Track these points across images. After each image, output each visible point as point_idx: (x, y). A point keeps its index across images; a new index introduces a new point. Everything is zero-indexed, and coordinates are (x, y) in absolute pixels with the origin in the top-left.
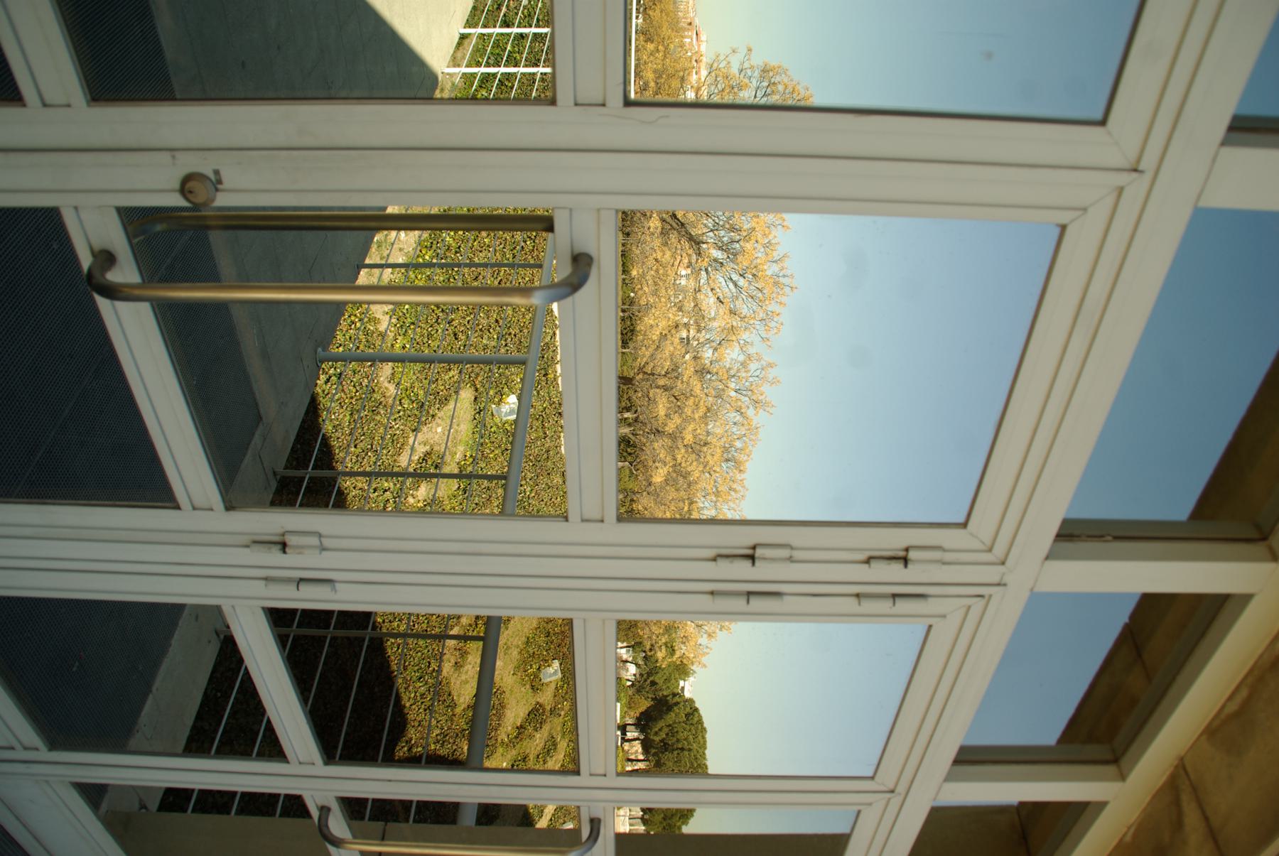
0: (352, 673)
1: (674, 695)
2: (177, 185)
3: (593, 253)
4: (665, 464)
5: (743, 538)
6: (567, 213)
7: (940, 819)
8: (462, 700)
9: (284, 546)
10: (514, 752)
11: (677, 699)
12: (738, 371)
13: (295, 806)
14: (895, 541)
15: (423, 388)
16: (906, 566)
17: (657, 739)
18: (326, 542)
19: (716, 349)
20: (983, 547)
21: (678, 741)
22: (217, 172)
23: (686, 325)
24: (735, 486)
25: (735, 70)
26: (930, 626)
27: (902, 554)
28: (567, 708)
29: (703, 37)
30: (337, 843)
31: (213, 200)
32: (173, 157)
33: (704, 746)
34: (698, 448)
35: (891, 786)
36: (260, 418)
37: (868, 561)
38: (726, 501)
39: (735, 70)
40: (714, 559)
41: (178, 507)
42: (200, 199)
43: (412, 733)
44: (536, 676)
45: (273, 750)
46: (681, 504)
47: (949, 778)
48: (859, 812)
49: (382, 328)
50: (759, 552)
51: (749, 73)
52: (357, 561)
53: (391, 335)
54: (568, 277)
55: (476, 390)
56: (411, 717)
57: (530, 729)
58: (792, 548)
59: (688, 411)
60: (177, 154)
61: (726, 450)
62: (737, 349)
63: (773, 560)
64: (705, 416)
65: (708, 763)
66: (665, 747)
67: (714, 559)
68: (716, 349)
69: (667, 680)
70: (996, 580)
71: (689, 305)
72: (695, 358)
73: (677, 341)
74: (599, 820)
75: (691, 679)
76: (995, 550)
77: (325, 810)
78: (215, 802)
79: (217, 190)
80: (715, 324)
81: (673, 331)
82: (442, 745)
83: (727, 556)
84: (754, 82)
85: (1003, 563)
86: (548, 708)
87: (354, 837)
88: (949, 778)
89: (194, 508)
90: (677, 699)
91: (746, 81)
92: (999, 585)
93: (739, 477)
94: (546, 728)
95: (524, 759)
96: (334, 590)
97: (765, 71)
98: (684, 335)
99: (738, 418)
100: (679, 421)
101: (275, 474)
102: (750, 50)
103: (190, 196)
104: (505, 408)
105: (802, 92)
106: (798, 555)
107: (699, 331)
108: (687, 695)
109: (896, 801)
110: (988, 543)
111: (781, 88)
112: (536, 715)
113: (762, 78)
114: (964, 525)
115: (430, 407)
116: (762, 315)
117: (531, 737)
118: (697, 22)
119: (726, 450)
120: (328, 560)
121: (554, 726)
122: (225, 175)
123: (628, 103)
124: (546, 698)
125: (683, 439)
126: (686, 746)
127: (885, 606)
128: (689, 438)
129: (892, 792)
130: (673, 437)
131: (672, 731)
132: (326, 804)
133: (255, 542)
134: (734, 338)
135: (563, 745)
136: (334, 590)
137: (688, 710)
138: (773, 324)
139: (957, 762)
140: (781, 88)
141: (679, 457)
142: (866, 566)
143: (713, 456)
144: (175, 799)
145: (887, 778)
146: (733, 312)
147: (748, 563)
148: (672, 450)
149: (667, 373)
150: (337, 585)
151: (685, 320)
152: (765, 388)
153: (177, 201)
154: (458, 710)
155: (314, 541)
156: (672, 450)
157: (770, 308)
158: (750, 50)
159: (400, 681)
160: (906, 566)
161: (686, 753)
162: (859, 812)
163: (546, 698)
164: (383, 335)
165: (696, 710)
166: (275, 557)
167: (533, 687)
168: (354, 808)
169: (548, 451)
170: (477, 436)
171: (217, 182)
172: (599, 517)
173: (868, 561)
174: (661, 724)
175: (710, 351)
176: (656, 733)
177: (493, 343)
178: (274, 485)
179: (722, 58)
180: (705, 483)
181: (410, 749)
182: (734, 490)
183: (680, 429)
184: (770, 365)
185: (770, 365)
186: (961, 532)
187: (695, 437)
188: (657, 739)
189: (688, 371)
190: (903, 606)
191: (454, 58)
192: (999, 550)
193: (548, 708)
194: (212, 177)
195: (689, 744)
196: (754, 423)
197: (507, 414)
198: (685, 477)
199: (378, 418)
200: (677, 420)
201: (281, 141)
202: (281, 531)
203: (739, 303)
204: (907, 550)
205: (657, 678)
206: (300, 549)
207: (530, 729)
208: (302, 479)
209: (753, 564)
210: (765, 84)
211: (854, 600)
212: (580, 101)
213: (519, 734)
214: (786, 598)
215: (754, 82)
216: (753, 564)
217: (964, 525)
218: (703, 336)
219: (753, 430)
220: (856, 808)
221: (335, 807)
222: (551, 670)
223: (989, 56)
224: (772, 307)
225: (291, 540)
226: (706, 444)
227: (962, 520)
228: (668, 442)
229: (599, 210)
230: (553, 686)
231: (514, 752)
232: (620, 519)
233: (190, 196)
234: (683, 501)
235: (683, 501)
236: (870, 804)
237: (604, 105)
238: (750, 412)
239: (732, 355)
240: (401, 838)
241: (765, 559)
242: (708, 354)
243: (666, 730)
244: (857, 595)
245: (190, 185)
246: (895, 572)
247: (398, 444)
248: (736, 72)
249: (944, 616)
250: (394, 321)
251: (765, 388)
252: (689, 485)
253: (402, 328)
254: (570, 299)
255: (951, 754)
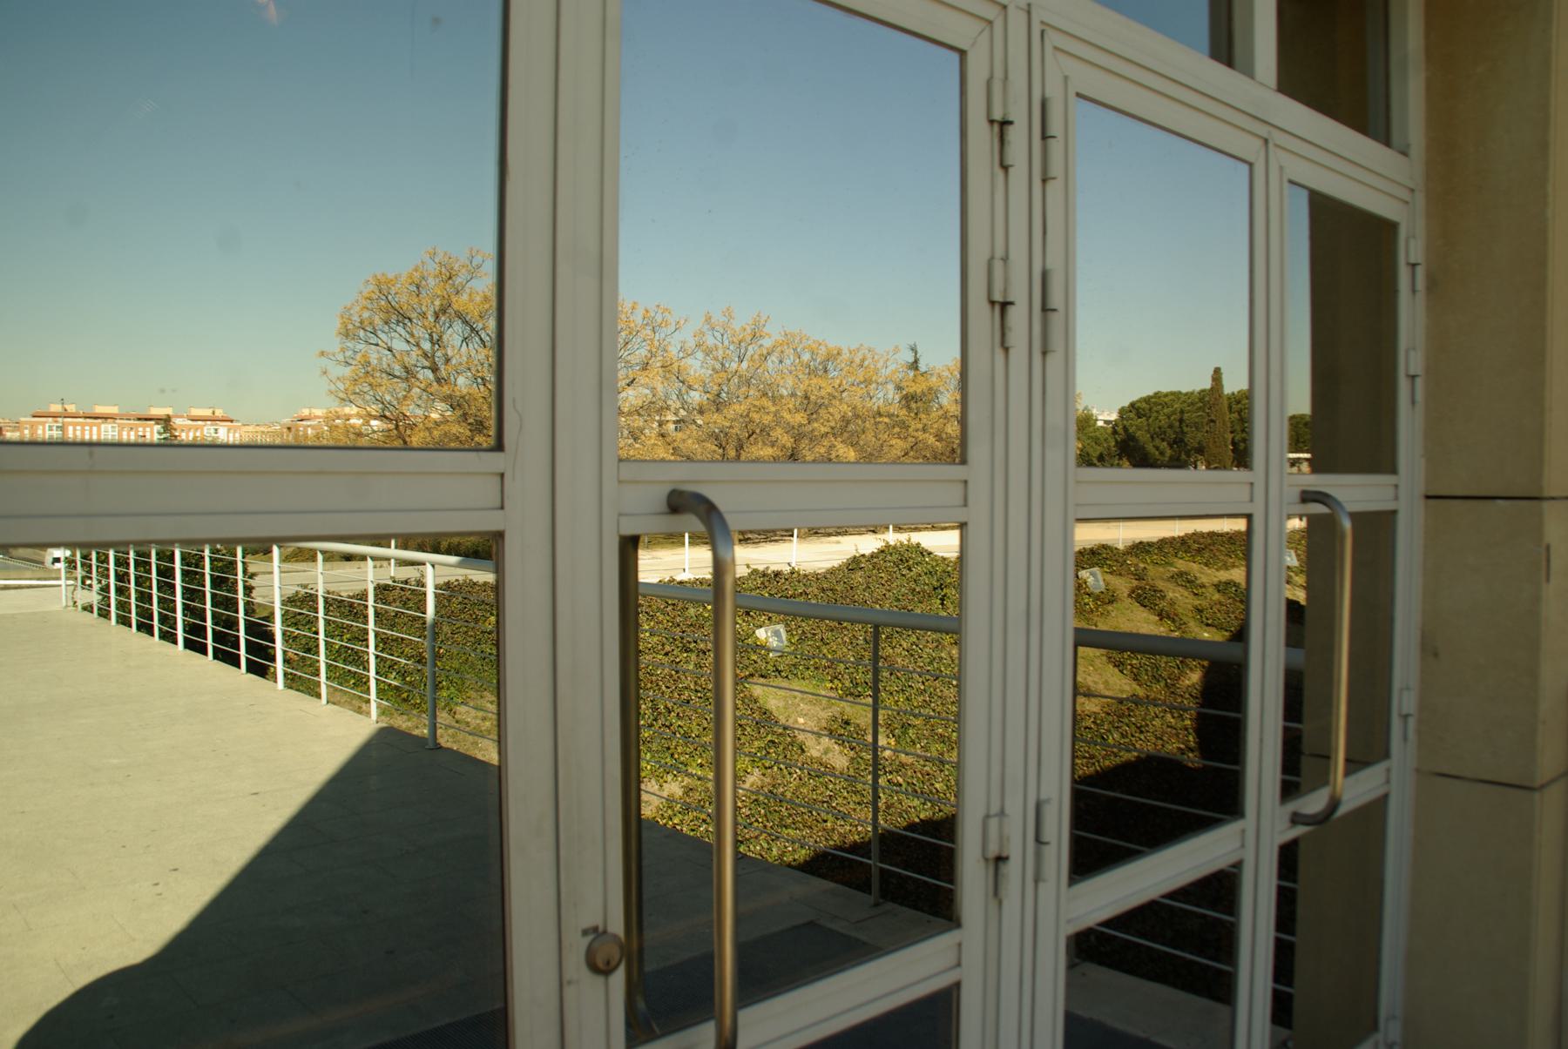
0: (1118, 809)
1: (1115, 432)
2: (600, 980)
3: (667, 489)
4: (832, 446)
5: (982, 317)
6: (623, 520)
7: (1292, 83)
8: (1127, 688)
9: (1000, 859)
10: (1192, 624)
11: (1120, 429)
12: (716, 359)
13: (1288, 856)
14: (981, 136)
15: (751, 743)
16: (1011, 123)
17: (1169, 452)
18: (995, 809)
19: (690, 387)
20: (986, 34)
21: (1171, 426)
22: (585, 933)
23: (661, 424)
24: (857, 361)
25: (347, 371)
26: (1078, 95)
27: (996, 128)
28: (1135, 560)
29: (306, 412)
30: (1334, 804)
31: (615, 936)
32: (569, 983)
33: (1176, 395)
34: (811, 406)
35: (1259, 143)
36: (811, 924)
37: (1005, 168)
38: (876, 372)
39: (347, 371)
40: (1006, 350)
41: (958, 985)
42: (615, 953)
43: (1172, 747)
44: (1097, 598)
45: (1220, 888)
46: (881, 427)
47: (1249, 73)
48: (1291, 182)
49: (679, 792)
50: (998, 297)
51: (349, 353)
52: (1011, 779)
53: (687, 780)
54: (697, 515)
55: (752, 675)
56: (1151, 748)
57: (1163, 604)
58: (992, 258)
59: (767, 419)
60: (567, 977)
61: (812, 372)
62: (689, 361)
63: (1006, 280)
64: (773, 399)
65: (1198, 389)
66: (1178, 442)
67: (1006, 350)
68: (690, 387)
69: (1097, 441)
70: (1023, 17)
71: (638, 422)
72: (701, 412)
73: (680, 435)
74: (1304, 492)
75: (1094, 411)
76: (991, 17)
77: (1296, 819)
78: (1284, 957)
79: (605, 932)
80: (660, 388)
81: (669, 439)
82: (1185, 710)
83: (1003, 335)
84: (359, 347)
85: (1005, 7)
86: (1135, 583)
87: (1325, 783)
88: (1249, 73)
89: (959, 965)
90: (1120, 429)
91: (358, 357)
92: (1029, 13)
93: (846, 355)
94: (1160, 584)
95: (1200, 611)
96: (1048, 801)
97: (346, 334)
98: (672, 426)
99: (774, 358)
100: (779, 431)
101: (876, 905)
102: (322, 353)
103: (613, 963)
104: (773, 642)
105: (371, 287)
106: (999, 253)
107: (668, 408)
108: (1114, 417)
109: (1278, 138)
110: (983, 25)
111: (366, 315)
112: (1146, 597)
113: (356, 337)
114: (962, 53)
115: (774, 733)
116: (648, 331)
117: (1172, 603)
118: (287, 421)
119: (812, 372)
120: (1014, 807)
121: (1157, 575)
122: (588, 923)
123: (499, 446)
124: (1123, 585)
125: (800, 425)
126: (1178, 416)
127: (1056, 147)
128: (800, 418)
129: (1266, 141)
130: (798, 438)
131: (1159, 434)
132: (1287, 818)
133: (996, 892)
134: (675, 366)
135: (1181, 564)
136: (1048, 801)
137: (1132, 415)
138: (659, 319)
139: (1229, 62)
140: (366, 315)
141: (823, 430)
142: (1011, 170)
143: (822, 387)
144: (1282, 1010)
145: (1249, 147)
146: (645, 367)
147: (1011, 310)
148: (814, 439)
149: (721, 446)
150: (1043, 796)
151: (655, 425)
152: (736, 326)
153: (619, 978)
154: (1141, 692)
155: (993, 824)
156: (814, 439)
157: (639, 320)
158: (322, 353)
159: (1107, 763)
160: (1011, 123)
161: (1186, 416)
162: (1291, 182)
163: (1123, 585)
164: (689, 790)
165: (1132, 405)
166: (1012, 870)
167: (1111, 602)
168: (1289, 790)
169: (823, 590)
170: (807, 674)
171: (596, 933)
172: (961, 486)
173: (1005, 168)
174: (1150, 448)
175: (692, 393)
176: (1162, 453)
177: (693, 656)
178: (890, 906)
179: (333, 387)
180: (854, 397)
181: (1191, 750)
182: (863, 360)
183: (789, 429)
184: (708, 319)
185: (708, 319)
186: (971, 58)
187: (798, 411)
188: (1169, 452)
189: (718, 420)
190: (1055, 127)
191: (359, 711)
192: (991, 12)
193: (1135, 583)
194: (590, 937)
195: (1174, 413)
196: (780, 338)
197: (780, 640)
198: (848, 422)
199: (789, 795)
200: (778, 433)
201: (549, 856)
202: (982, 863)
203: (634, 359)
204: (992, 122)
205: (1095, 454)
206: (1002, 839)
207: (1163, 604)
208: (882, 870)
209: (1011, 303)
210: (362, 333)
211: (1050, 185)
212: (498, 504)
213: (1168, 617)
214: (1049, 266)
215: (359, 347)
216: (1011, 303)
217: (962, 53)
218: (674, 403)
219: (789, 340)
220: (1286, 184)
221: (1292, 806)
222: (1091, 580)
223: (436, 21)
224: (638, 318)
225: (993, 850)
226: (807, 397)
227: (955, 57)
228: (804, 443)
229: (620, 482)
230: (1108, 577)
231: (1192, 624)
232: (964, 462)
233: (613, 963)
234: (877, 423)
235: (877, 423)
236: (1281, 168)
237: (502, 475)
238: (767, 343)
239: (696, 367)
240: (1327, 731)
241: (1005, 290)
242: (696, 397)
243: (1157, 442)
244: (1044, 181)
245: (601, 965)
246: (1017, 136)
247: (821, 771)
248: (349, 369)
249: (1066, 78)
250: (670, 777)
251: (736, 326)
252: (857, 416)
253: (679, 769)
254: (727, 517)
255: (1221, 69)
